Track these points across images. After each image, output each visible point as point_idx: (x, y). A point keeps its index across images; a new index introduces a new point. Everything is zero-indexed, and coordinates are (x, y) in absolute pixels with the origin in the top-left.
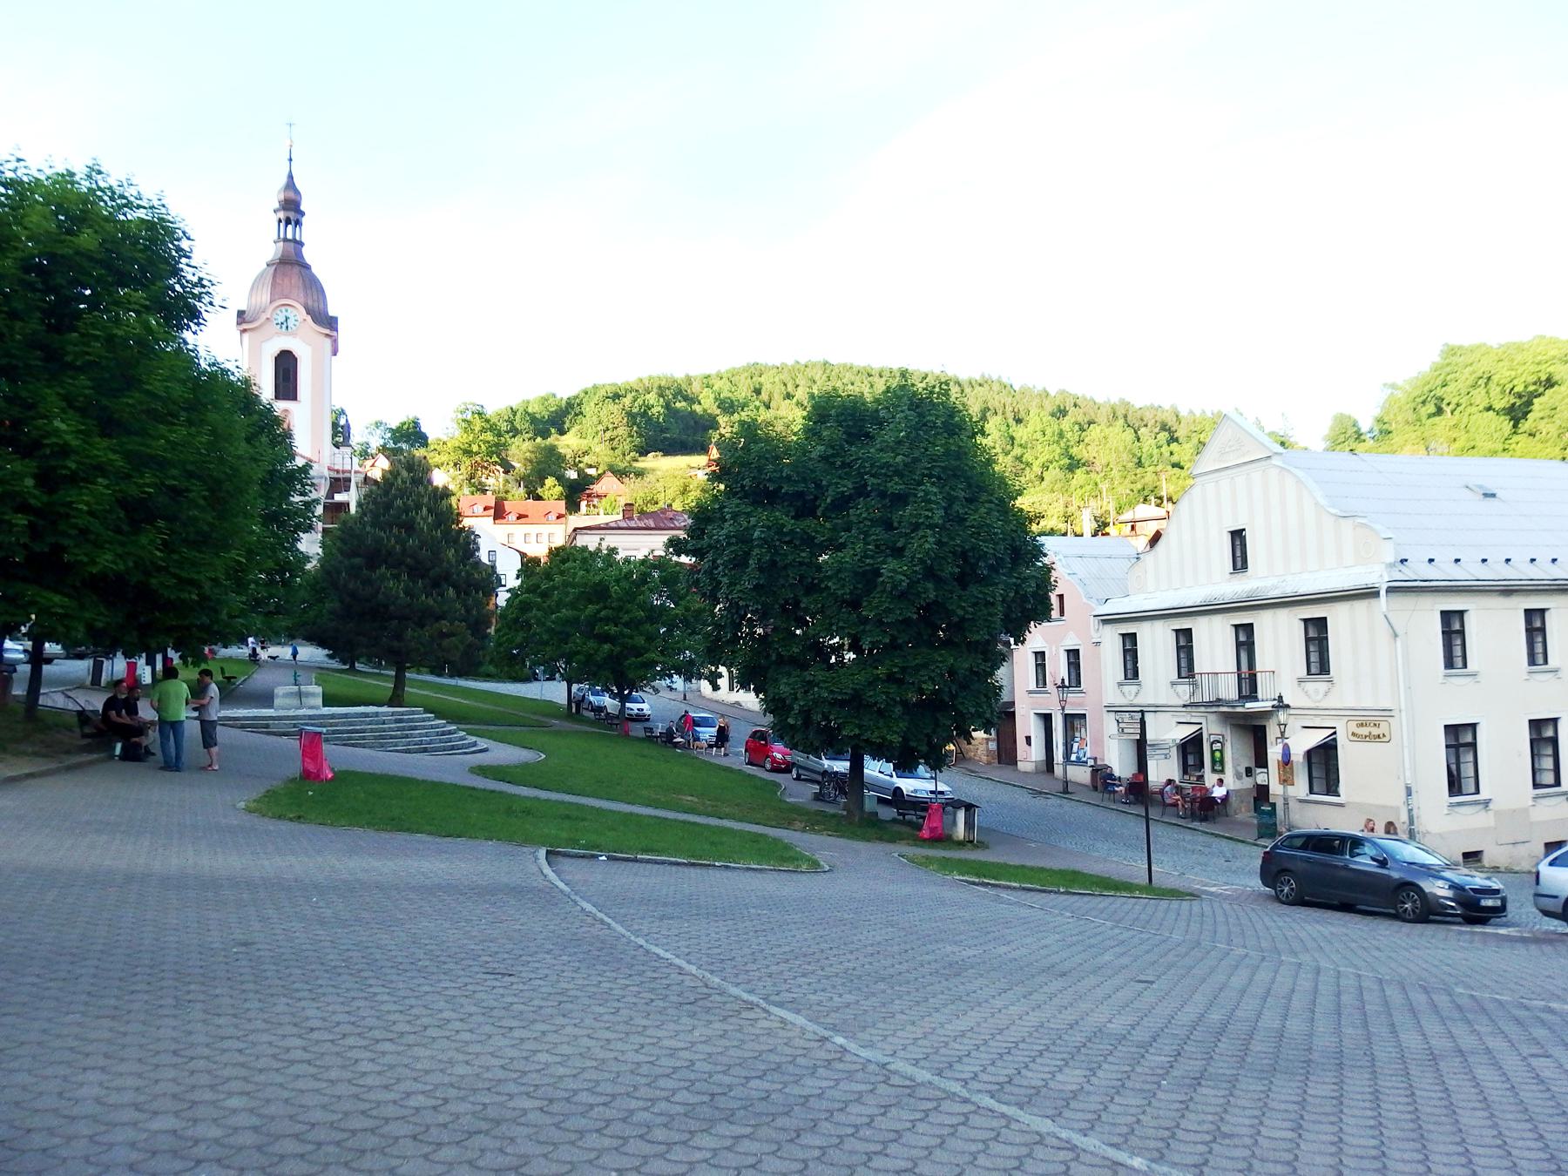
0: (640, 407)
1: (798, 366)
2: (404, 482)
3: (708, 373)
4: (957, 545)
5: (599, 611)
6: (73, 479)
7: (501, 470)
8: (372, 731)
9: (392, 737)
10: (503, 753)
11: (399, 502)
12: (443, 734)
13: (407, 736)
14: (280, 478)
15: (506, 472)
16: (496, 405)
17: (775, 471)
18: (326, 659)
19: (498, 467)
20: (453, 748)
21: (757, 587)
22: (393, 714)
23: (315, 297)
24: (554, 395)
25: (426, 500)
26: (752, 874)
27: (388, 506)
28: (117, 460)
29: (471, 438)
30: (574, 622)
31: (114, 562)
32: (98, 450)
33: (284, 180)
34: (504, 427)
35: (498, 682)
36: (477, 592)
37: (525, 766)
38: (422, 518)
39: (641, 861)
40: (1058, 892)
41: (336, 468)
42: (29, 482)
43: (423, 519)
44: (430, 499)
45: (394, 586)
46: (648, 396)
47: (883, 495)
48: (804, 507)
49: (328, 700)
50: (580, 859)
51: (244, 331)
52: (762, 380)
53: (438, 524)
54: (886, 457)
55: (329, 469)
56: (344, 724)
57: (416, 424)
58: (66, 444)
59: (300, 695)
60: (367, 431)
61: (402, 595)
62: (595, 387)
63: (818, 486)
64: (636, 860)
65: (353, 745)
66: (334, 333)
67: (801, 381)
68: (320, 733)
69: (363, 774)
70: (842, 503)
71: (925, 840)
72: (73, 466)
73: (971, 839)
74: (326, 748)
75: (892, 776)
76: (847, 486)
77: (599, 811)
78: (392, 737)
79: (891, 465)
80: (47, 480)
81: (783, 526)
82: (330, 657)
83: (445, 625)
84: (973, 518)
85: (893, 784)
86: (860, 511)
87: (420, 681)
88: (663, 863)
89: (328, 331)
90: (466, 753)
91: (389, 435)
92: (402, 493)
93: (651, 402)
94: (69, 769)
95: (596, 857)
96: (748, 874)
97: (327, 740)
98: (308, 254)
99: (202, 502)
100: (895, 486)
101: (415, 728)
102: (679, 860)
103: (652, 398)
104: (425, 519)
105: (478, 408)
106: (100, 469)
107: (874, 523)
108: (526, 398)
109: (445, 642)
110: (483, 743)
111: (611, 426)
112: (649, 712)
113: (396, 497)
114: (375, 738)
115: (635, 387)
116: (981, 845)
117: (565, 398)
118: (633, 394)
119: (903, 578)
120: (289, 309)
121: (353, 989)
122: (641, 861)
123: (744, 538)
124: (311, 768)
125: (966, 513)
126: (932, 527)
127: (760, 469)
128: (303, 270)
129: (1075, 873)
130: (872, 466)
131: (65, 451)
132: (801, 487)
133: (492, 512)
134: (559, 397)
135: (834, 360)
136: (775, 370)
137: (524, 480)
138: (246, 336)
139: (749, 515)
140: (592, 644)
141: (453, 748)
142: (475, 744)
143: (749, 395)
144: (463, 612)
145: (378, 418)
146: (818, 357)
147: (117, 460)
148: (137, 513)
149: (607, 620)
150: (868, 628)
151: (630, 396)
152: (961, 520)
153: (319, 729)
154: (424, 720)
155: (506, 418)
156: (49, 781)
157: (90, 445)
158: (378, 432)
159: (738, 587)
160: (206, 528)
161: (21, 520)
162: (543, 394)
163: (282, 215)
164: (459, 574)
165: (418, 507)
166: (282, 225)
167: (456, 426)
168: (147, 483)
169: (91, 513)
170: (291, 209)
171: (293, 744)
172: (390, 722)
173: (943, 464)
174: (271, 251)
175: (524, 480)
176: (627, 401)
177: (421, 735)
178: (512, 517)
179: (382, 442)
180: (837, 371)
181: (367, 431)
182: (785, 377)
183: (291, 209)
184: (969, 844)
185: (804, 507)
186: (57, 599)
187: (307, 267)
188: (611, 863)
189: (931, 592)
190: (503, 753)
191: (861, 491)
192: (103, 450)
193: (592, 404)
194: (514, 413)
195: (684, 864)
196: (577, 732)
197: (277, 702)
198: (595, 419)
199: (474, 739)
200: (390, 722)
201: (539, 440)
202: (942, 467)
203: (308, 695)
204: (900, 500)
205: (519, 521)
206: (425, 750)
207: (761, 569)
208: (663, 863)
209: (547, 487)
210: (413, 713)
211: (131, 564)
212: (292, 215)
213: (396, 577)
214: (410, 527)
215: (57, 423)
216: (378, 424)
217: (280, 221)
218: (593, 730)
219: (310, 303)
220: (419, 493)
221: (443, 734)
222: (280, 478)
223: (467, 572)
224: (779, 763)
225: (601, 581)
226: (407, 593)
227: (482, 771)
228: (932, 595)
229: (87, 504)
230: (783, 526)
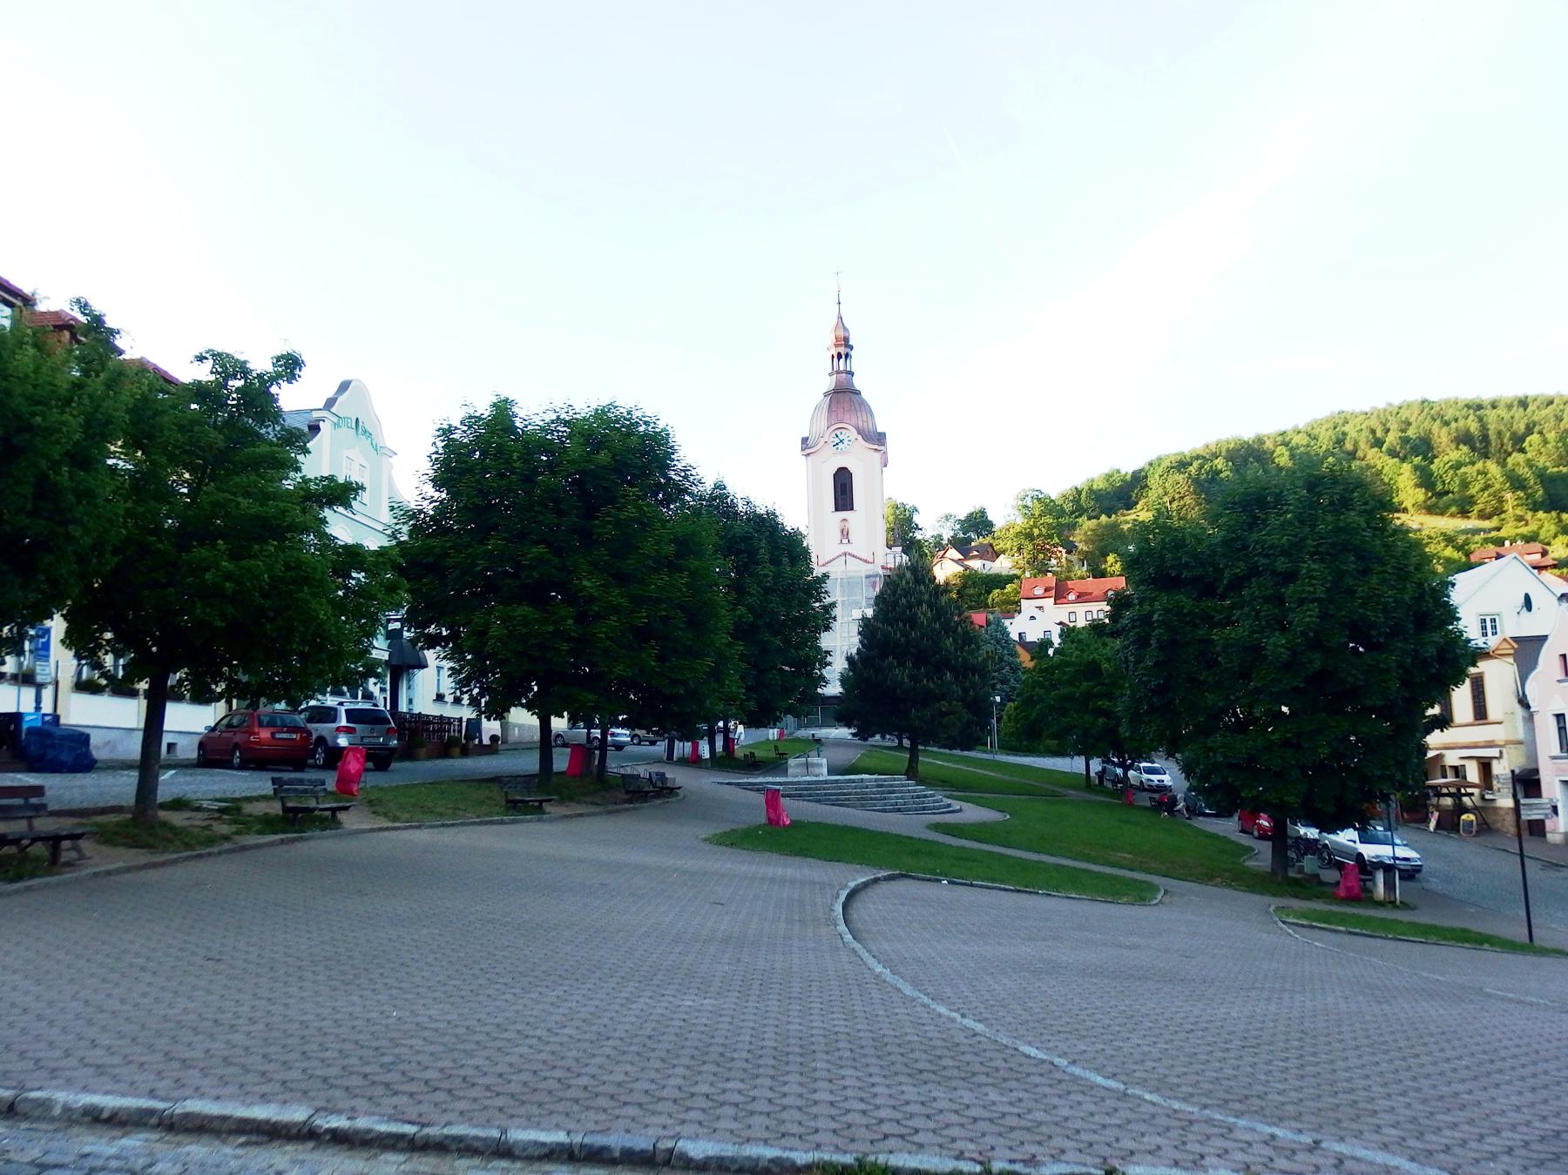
0: (1207, 473)
1: (1391, 409)
2: (908, 583)
3: (1283, 429)
4: (1344, 616)
5: (1093, 688)
6: (598, 617)
7: (1064, 551)
8: (856, 794)
9: (871, 799)
10: (972, 813)
11: (904, 601)
12: (918, 797)
13: (885, 799)
14: (799, 589)
15: (1069, 552)
16: (1057, 487)
17: (1174, 559)
18: (850, 737)
19: (1060, 549)
20: (924, 809)
21: (1156, 664)
22: (876, 780)
23: (865, 418)
24: (1118, 471)
25: (926, 597)
26: (1071, 901)
27: (895, 604)
28: (624, 602)
29: (1031, 523)
30: (1069, 698)
31: (624, 671)
32: (612, 596)
33: (835, 320)
34: (1068, 507)
35: (1038, 756)
36: (973, 675)
37: (983, 826)
38: (922, 613)
39: (976, 886)
40: (1386, 938)
41: (889, 566)
42: (570, 622)
43: (924, 614)
44: (930, 596)
45: (901, 674)
46: (1216, 462)
47: (1274, 573)
48: (1206, 589)
49: (830, 772)
50: (926, 882)
51: (808, 454)
52: (1346, 428)
53: (937, 618)
54: (1274, 539)
55: (883, 568)
56: (834, 788)
57: (983, 513)
58: (591, 595)
59: (807, 765)
60: (937, 525)
61: (906, 680)
62: (1160, 459)
63: (1217, 569)
64: (972, 885)
65: (839, 805)
66: (882, 448)
67: (1393, 426)
68: (779, 790)
69: (836, 826)
70: (1237, 584)
71: (1343, 899)
72: (597, 609)
73: (1392, 899)
74: (785, 802)
75: (1355, 842)
76: (1240, 568)
77: (1002, 855)
78: (871, 799)
79: (1277, 547)
80: (581, 618)
81: (1183, 607)
82: (854, 735)
83: (944, 705)
84: (1362, 590)
85: (1356, 849)
86: (1252, 590)
87: (935, 759)
88: (994, 888)
89: (876, 447)
90: (935, 814)
91: (958, 526)
92: (907, 593)
93: (1219, 467)
94: (610, 813)
95: (940, 881)
96: (1066, 901)
97: (784, 796)
98: (858, 383)
99: (682, 626)
100: (1282, 564)
101: (894, 792)
102: (1007, 887)
103: (1219, 463)
104: (924, 614)
105: (1037, 493)
106: (616, 609)
107: (1266, 600)
108: (1090, 477)
109: (945, 720)
110: (956, 805)
111: (1177, 496)
112: (1170, 784)
113: (900, 596)
114: (858, 799)
115: (1201, 453)
116: (1405, 906)
117: (1130, 471)
118: (1200, 461)
119: (1283, 650)
120: (844, 431)
121: (1045, 1123)
122: (976, 886)
123: (1146, 620)
124: (772, 816)
125: (1356, 585)
126: (1315, 600)
127: (1162, 558)
128: (853, 396)
129: (1465, 931)
130: (1262, 547)
131: (591, 599)
132: (1199, 572)
133: (1053, 593)
134: (1123, 472)
135: (1433, 397)
136: (1363, 417)
137: (1086, 557)
138: (809, 458)
139: (1154, 599)
140: (1087, 718)
141: (924, 809)
142: (949, 806)
143: (1331, 447)
144: (960, 692)
145: (947, 512)
146: (1415, 396)
147: (624, 602)
148: (643, 635)
149: (1100, 696)
150: (1261, 697)
151: (1196, 464)
152: (1351, 592)
153: (778, 787)
154: (903, 786)
155: (1071, 498)
156: (588, 820)
157: (607, 593)
158: (949, 524)
159: (1142, 665)
160: (689, 643)
161: (565, 647)
162: (1107, 471)
163: (834, 352)
164: (956, 659)
165: (920, 603)
166: (835, 359)
167: (1017, 513)
168: (642, 617)
169: (608, 638)
170: (844, 348)
171: (760, 798)
172: (872, 787)
173: (1330, 541)
174: (828, 383)
175: (1086, 557)
176: (1193, 469)
177: (897, 798)
178: (1072, 597)
179: (952, 533)
180: (1439, 408)
181: (937, 525)
182: (1374, 423)
183: (844, 348)
184: (1390, 906)
185: (1206, 589)
186: (591, 696)
187: (858, 393)
188: (951, 886)
189: (1317, 661)
190: (972, 813)
191: (1254, 571)
192: (616, 596)
193: (1157, 476)
194: (1079, 492)
195: (1012, 890)
196: (1090, 802)
197: (790, 771)
198: (1161, 491)
199: (949, 801)
200: (872, 787)
201: (1104, 518)
202: (1330, 544)
203: (814, 765)
204: (1290, 577)
205: (1080, 600)
206: (899, 810)
207: (1161, 648)
208: (994, 888)
209: (1109, 564)
210: (895, 780)
211: (637, 671)
212: (842, 350)
213: (901, 664)
214: (912, 621)
215: (585, 583)
216: (947, 518)
217: (833, 357)
218: (1102, 799)
219: (860, 423)
220: (921, 591)
221: (918, 797)
222: (799, 589)
223: (964, 658)
224: (1267, 831)
225: (1093, 660)
226: (911, 678)
227: (937, 827)
228: (1317, 665)
229: (606, 633)
230: (1183, 607)
